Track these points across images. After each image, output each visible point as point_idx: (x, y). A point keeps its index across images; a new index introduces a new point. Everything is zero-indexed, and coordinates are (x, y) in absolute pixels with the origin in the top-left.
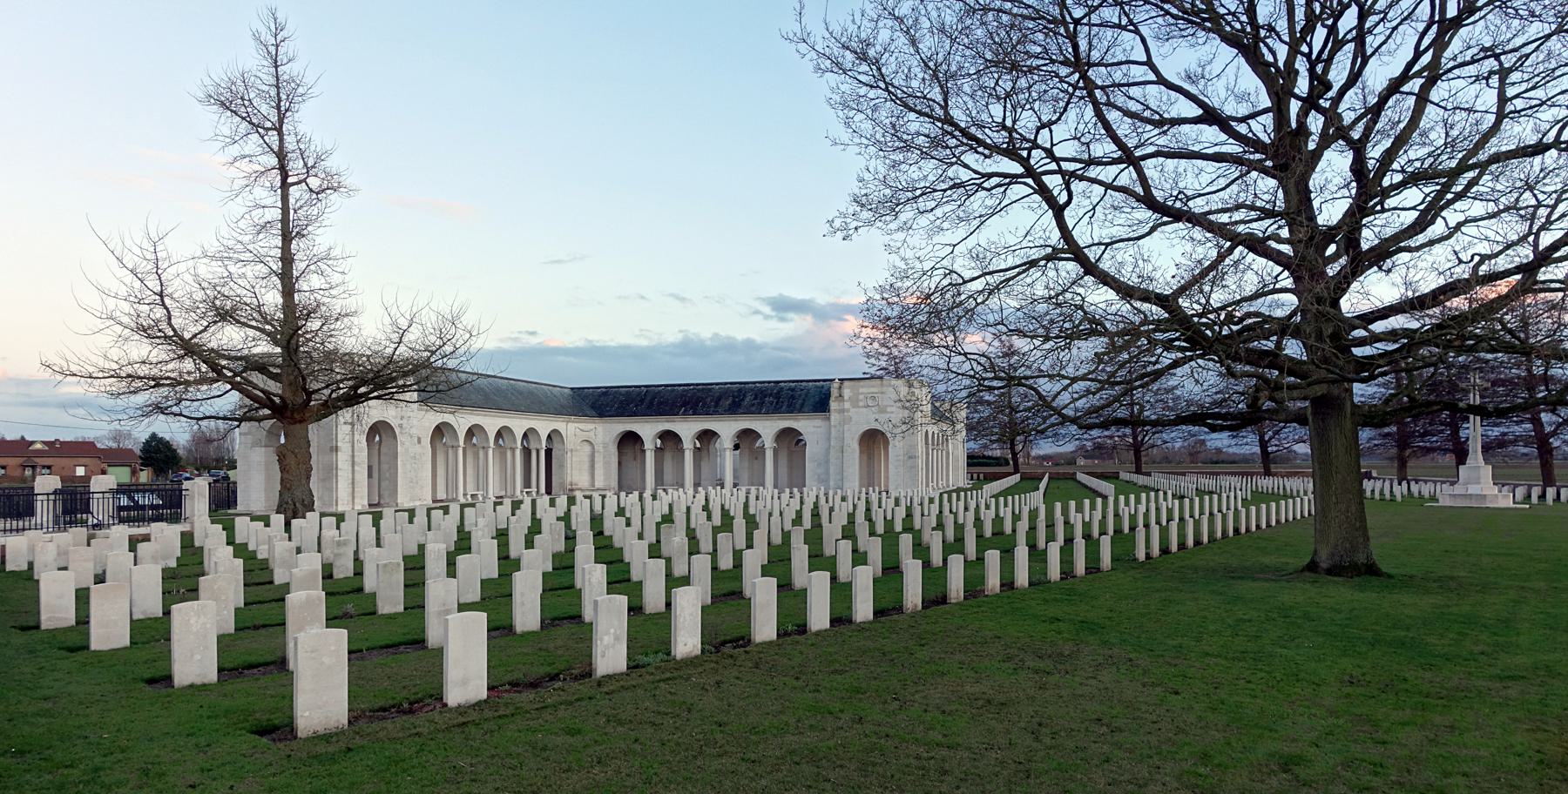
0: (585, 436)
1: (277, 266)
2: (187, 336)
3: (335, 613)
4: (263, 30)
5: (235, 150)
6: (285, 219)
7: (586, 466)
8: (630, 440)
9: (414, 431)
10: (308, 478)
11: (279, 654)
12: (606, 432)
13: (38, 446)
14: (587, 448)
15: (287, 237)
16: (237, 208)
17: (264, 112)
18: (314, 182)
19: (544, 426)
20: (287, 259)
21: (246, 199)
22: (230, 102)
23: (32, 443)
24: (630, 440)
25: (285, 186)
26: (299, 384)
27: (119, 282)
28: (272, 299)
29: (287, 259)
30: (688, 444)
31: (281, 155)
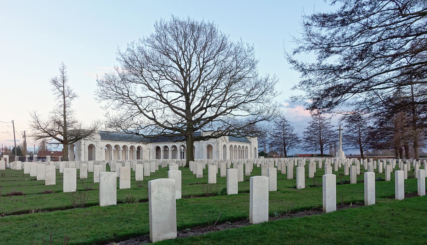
0: (148, 147)
1: (63, 113)
2: (169, 101)
3: (97, 191)
4: (61, 67)
5: (55, 92)
6: (64, 104)
7: (148, 155)
8: (158, 148)
9: (100, 146)
10: (68, 155)
11: (148, 231)
12: (152, 146)
13: (52, 153)
14: (148, 150)
15: (65, 108)
16: (57, 101)
17: (60, 84)
18: (70, 96)
19: (136, 145)
20: (65, 112)
21: (57, 101)
22: (55, 82)
23: (51, 152)
24: (158, 148)
25: (64, 97)
26: (71, 137)
27: (32, 120)
28: (62, 119)
29: (65, 112)
30: (162, 149)
31: (63, 93)
